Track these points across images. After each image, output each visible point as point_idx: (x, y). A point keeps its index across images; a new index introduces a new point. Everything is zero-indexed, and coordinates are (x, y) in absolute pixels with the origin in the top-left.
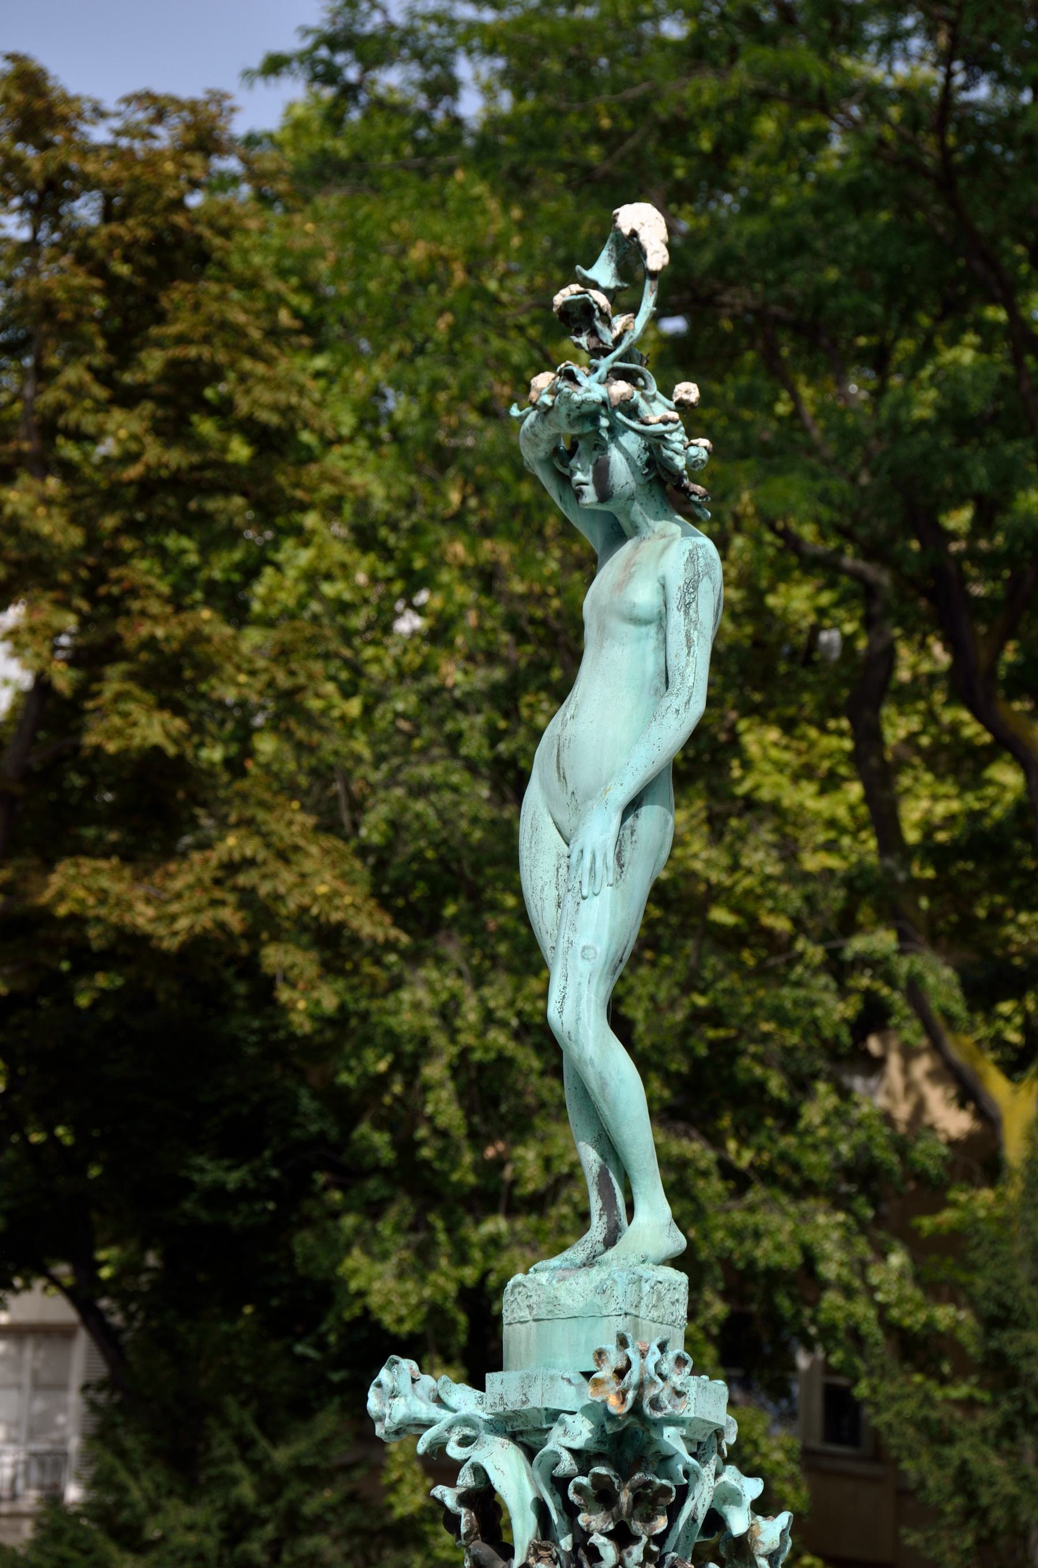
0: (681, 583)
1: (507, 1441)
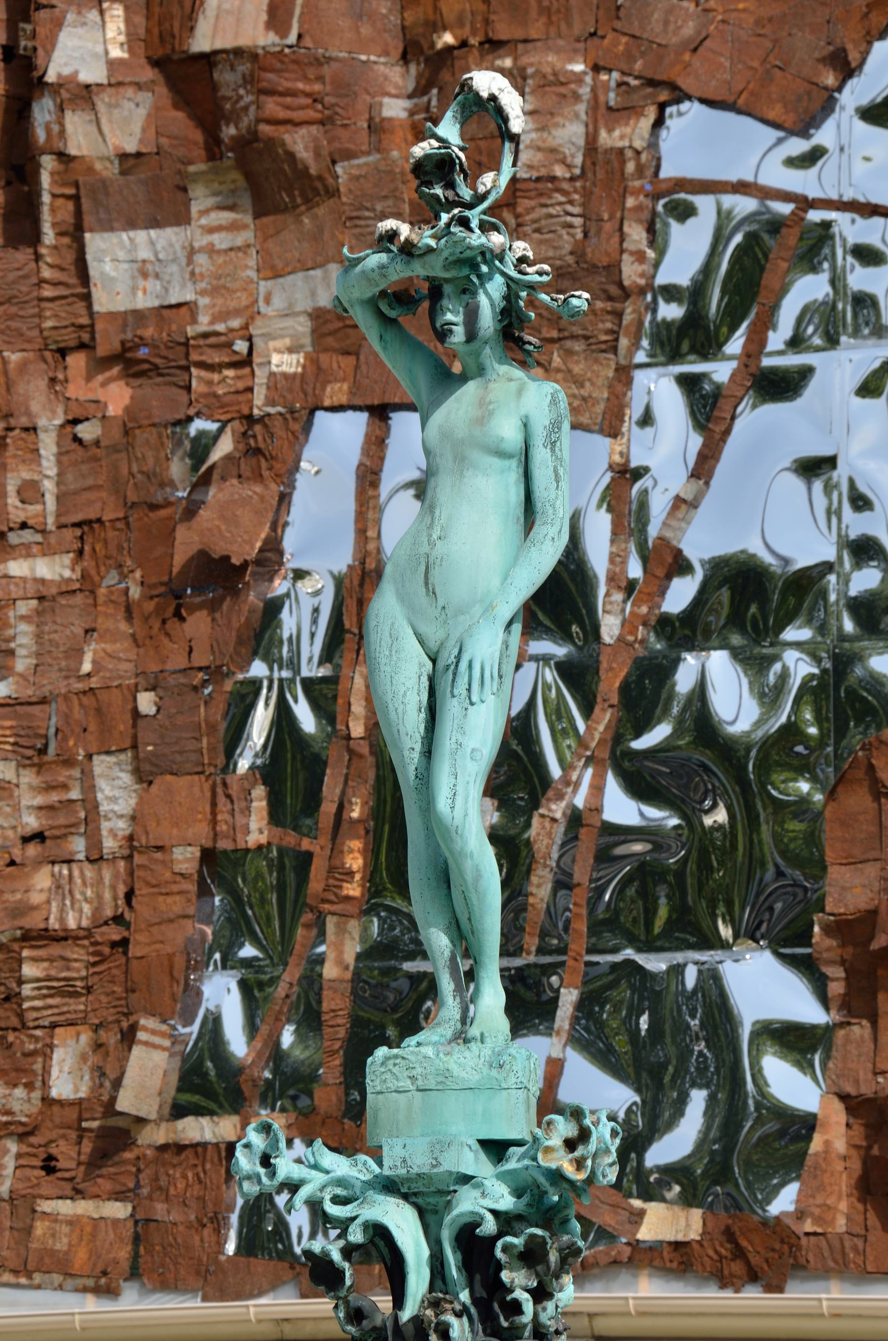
0: (547, 423)
1: (401, 1201)
